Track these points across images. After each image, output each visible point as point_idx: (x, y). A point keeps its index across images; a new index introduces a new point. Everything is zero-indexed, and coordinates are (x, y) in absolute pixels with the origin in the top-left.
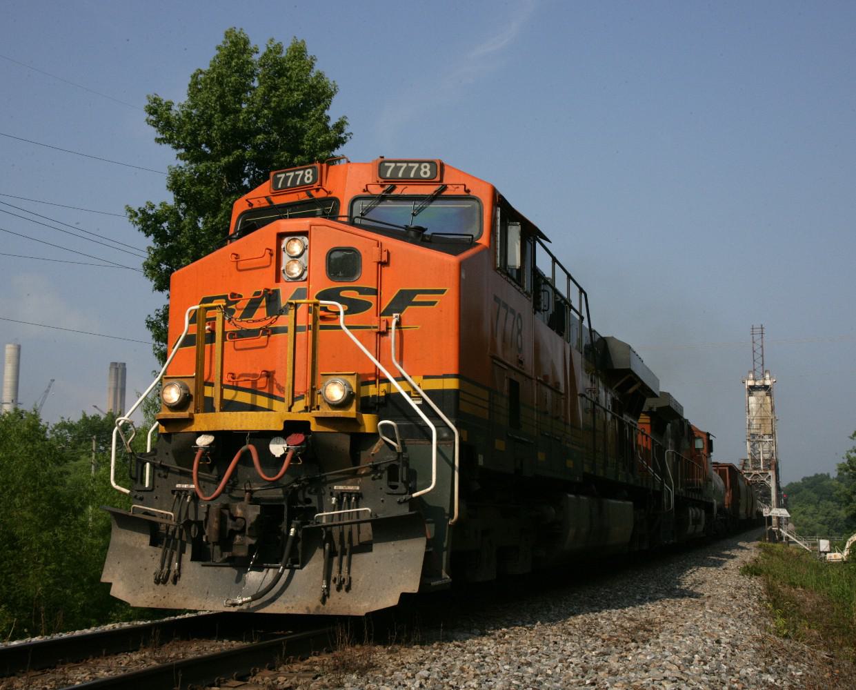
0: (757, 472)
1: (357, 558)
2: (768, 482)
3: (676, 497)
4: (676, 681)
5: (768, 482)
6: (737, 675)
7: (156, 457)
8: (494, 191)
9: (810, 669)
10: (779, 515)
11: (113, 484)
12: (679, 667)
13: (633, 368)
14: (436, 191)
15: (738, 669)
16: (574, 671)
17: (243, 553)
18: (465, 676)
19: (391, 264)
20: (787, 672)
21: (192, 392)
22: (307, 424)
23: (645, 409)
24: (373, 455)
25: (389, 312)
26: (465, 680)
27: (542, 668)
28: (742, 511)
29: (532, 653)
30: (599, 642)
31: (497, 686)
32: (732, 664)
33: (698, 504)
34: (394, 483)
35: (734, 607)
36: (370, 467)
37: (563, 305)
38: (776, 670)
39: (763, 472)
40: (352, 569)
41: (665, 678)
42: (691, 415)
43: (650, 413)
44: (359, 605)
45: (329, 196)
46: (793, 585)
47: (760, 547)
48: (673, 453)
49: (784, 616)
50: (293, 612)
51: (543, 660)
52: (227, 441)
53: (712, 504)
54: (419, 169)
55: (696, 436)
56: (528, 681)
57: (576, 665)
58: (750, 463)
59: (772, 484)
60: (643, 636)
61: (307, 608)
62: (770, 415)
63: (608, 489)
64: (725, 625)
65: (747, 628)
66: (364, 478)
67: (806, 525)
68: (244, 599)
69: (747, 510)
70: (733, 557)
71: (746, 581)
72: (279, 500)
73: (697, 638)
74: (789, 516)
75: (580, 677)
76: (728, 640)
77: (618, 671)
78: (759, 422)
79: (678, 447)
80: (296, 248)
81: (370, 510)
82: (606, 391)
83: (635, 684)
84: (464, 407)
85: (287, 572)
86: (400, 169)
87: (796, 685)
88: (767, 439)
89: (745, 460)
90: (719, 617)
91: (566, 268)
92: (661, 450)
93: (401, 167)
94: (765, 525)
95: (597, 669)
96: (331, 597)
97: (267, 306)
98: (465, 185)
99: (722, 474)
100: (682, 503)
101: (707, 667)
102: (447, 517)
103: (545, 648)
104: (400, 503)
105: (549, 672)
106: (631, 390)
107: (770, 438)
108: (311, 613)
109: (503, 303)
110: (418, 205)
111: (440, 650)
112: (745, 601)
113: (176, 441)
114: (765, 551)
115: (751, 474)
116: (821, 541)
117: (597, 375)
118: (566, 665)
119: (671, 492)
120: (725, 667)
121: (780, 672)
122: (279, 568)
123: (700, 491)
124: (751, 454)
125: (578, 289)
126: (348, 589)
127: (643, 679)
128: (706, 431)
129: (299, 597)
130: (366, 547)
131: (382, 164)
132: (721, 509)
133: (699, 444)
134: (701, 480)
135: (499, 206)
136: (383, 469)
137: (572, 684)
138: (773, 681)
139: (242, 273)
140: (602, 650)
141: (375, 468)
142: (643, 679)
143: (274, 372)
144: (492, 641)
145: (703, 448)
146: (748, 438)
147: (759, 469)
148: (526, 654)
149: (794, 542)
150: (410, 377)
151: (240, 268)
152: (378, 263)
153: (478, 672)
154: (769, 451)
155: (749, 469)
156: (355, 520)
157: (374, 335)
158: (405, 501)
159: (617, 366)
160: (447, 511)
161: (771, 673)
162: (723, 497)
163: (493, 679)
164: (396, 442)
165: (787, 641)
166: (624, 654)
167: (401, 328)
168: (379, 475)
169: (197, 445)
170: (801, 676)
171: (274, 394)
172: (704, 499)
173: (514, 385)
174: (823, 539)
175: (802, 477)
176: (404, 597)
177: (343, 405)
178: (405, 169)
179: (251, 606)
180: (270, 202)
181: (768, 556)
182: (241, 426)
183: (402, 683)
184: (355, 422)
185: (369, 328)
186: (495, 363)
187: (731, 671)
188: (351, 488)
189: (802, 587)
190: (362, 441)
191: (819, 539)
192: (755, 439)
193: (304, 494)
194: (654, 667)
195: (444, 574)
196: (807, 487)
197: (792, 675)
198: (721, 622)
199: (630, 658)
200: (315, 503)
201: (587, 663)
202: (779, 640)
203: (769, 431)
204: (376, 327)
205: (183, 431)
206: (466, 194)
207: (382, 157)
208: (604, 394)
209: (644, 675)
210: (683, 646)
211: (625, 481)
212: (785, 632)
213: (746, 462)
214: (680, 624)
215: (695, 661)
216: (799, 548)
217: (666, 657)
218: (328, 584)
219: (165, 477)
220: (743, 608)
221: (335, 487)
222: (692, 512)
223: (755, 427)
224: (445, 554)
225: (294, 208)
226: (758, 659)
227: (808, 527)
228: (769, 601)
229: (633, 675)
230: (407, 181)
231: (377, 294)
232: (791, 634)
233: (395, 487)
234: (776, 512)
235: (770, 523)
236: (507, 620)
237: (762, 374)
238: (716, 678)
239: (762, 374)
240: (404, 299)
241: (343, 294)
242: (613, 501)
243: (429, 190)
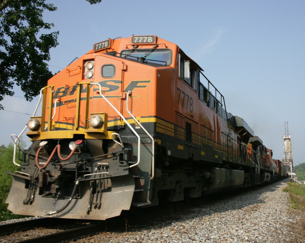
0: (287, 163)
1: (105, 194)
3: (260, 169)
4: (265, 222)
5: (290, 165)
6: (282, 220)
8: (177, 47)
9: (302, 217)
11: (14, 162)
12: (266, 218)
14: (154, 47)
15: (282, 218)
16: (236, 219)
18: (205, 221)
20: (295, 218)
22: (83, 135)
23: (250, 141)
24: (113, 149)
25: (126, 90)
26: (205, 222)
27: (227, 218)
28: (282, 174)
29: (224, 214)
30: (243, 211)
31: (215, 224)
32: (280, 216)
33: (268, 172)
35: (281, 201)
36: (111, 154)
37: (216, 102)
38: (292, 218)
41: (262, 221)
42: (266, 144)
43: (252, 143)
44: (103, 215)
45: (113, 51)
46: (297, 194)
47: (288, 184)
48: (259, 155)
49: (294, 203)
51: (227, 216)
52: (52, 143)
53: (273, 172)
54: (148, 39)
55: (267, 151)
56: (223, 222)
57: (237, 217)
58: (285, 160)
60: (255, 209)
63: (235, 166)
64: (278, 206)
65: (284, 206)
66: (110, 159)
67: (300, 177)
69: (283, 173)
70: (279, 187)
71: (284, 193)
72: (74, 169)
73: (271, 210)
74: (296, 175)
75: (238, 221)
76: (279, 210)
77: (249, 219)
78: (287, 148)
79: (261, 154)
80: (90, 66)
82: (235, 134)
83: (253, 222)
84: (158, 130)
85: (74, 200)
87: (298, 222)
88: (289, 153)
90: (276, 203)
91: (204, 77)
92: (255, 154)
95: (243, 219)
96: (92, 211)
98: (165, 44)
99: (276, 163)
100: (262, 171)
101: (273, 218)
102: (150, 176)
103: (228, 213)
104: (124, 170)
105: (229, 220)
106: (244, 134)
107: (290, 153)
109: (182, 91)
111: (199, 214)
112: (284, 199)
114: (289, 185)
117: (232, 129)
118: (234, 217)
119: (258, 167)
120: (278, 217)
121: (293, 218)
123: (269, 168)
124: (285, 158)
125: (220, 95)
126: (99, 208)
127: (255, 221)
128: (271, 149)
129: (78, 211)
131: (133, 38)
132: (275, 173)
133: (268, 153)
134: (269, 164)
135: (180, 53)
136: (117, 155)
137: (236, 223)
138: (291, 221)
139: (71, 77)
140: (244, 213)
142: (255, 221)
144: (213, 211)
147: (287, 162)
148: (223, 215)
149: (297, 182)
150: (135, 117)
151: (70, 75)
153: (209, 220)
155: (285, 162)
156: (102, 177)
157: (120, 100)
158: (127, 169)
159: (238, 126)
160: (150, 174)
161: (291, 219)
162: (276, 169)
163: (213, 222)
164: (120, 142)
165: (295, 210)
166: (250, 214)
167: (132, 97)
169: (39, 145)
170: (299, 219)
172: (270, 170)
173: (188, 126)
176: (123, 212)
177: (98, 127)
179: (58, 215)
181: (290, 186)
182: (56, 137)
183: (188, 223)
184: (103, 134)
185: (118, 97)
186: (177, 114)
187: (280, 218)
188: (104, 164)
189: (299, 195)
190: (107, 143)
192: (286, 153)
193: (86, 167)
194: (259, 218)
195: (148, 201)
196: (301, 167)
197: (297, 219)
198: (277, 205)
199: (252, 215)
201: (240, 217)
202: (293, 210)
203: (290, 151)
204: (121, 97)
206: (166, 48)
207: (133, 35)
208: (234, 135)
209: (256, 220)
210: (267, 212)
211: (241, 164)
212: (295, 207)
214: (266, 206)
215: (270, 216)
217: (262, 215)
218: (91, 206)
220: (283, 201)
221: (98, 163)
222: (266, 174)
223: (286, 150)
224: (149, 192)
226: (288, 215)
228: (290, 199)
229: (253, 220)
232: (296, 208)
233: (122, 163)
234: (291, 174)
235: (290, 177)
236: (217, 205)
238: (276, 220)
239: (288, 135)
241: (107, 83)
242: (234, 170)
243: (151, 47)
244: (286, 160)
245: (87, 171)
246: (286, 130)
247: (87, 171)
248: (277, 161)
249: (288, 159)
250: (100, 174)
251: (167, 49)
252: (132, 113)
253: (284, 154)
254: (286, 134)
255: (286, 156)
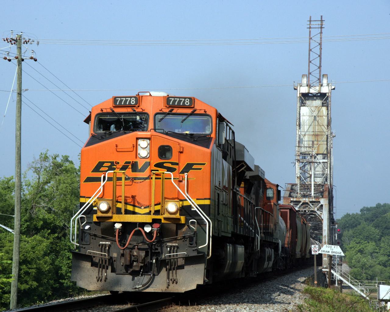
0: (307, 200)
1: (179, 271)
2: (319, 212)
3: (261, 240)
5: (319, 212)
7: (90, 231)
10: (330, 254)
13: (245, 160)
17: (137, 269)
19: (184, 153)
21: (111, 206)
22: (160, 220)
24: (183, 232)
25: (183, 172)
28: (298, 250)
34: (191, 243)
39: (314, 200)
40: (177, 275)
44: (181, 289)
45: (143, 111)
47: (306, 291)
50: (156, 291)
52: (127, 227)
53: (278, 244)
54: (184, 101)
55: (268, 187)
58: (298, 188)
59: (325, 216)
61: (162, 290)
62: (325, 130)
66: (180, 241)
67: (363, 266)
68: (139, 286)
69: (302, 248)
74: (343, 254)
81: (186, 253)
86: (171, 101)
88: (320, 159)
89: (293, 185)
93: (177, 100)
94: (313, 265)
97: (132, 168)
102: (206, 256)
104: (194, 250)
107: (324, 158)
108: (164, 292)
110: (184, 117)
113: (103, 225)
114: (313, 297)
115: (300, 202)
116: (382, 286)
122: (150, 275)
124: (300, 178)
126: (177, 283)
130: (181, 267)
139: (119, 153)
141: (184, 237)
143: (136, 196)
145: (273, 197)
146: (298, 158)
147: (309, 196)
149: (349, 287)
152: (179, 152)
154: (323, 174)
155: (298, 196)
157: (177, 181)
160: (206, 254)
168: (186, 239)
171: (136, 205)
174: (384, 284)
175: (362, 207)
176: (198, 286)
178: (173, 101)
180: (113, 111)
186: (216, 189)
188: (174, 244)
190: (180, 226)
191: (380, 283)
193: (155, 247)
196: (367, 220)
200: (159, 250)
203: (323, 149)
204: (178, 179)
205: (107, 221)
206: (205, 113)
207: (168, 95)
213: (294, 187)
216: (353, 294)
219: (95, 239)
223: (306, 144)
225: (125, 115)
227: (366, 269)
230: (179, 107)
231: (178, 165)
233: (191, 244)
235: (320, 263)
237: (319, 79)
239: (319, 79)
240: (189, 167)
241: (165, 165)
243: (189, 111)
244: (306, 187)
245: (156, 251)
246: (314, 44)
247: (156, 251)
248: (287, 212)
249: (313, 183)
250: (173, 253)
251: (206, 114)
252: (188, 194)
253: (298, 160)
254: (310, 73)
255: (305, 172)
